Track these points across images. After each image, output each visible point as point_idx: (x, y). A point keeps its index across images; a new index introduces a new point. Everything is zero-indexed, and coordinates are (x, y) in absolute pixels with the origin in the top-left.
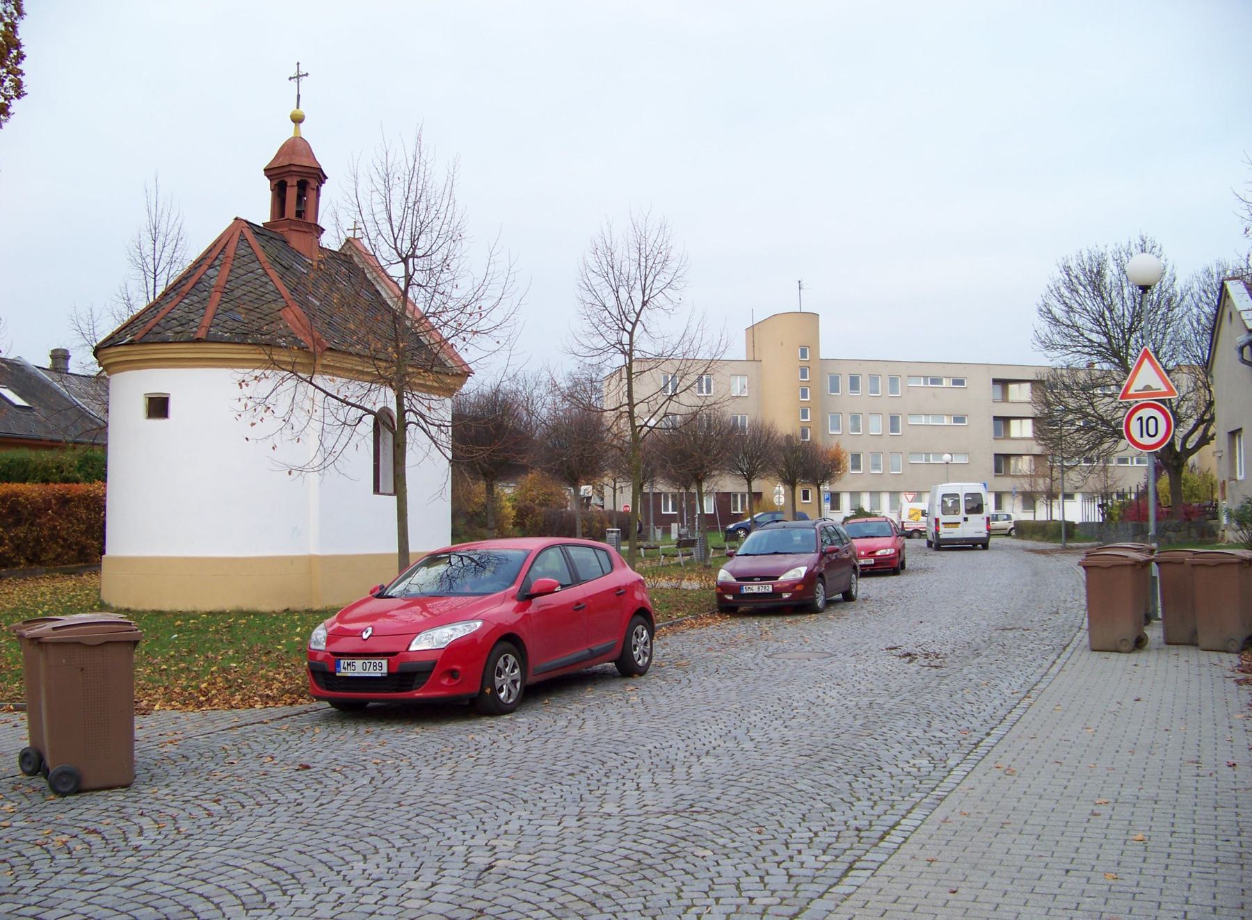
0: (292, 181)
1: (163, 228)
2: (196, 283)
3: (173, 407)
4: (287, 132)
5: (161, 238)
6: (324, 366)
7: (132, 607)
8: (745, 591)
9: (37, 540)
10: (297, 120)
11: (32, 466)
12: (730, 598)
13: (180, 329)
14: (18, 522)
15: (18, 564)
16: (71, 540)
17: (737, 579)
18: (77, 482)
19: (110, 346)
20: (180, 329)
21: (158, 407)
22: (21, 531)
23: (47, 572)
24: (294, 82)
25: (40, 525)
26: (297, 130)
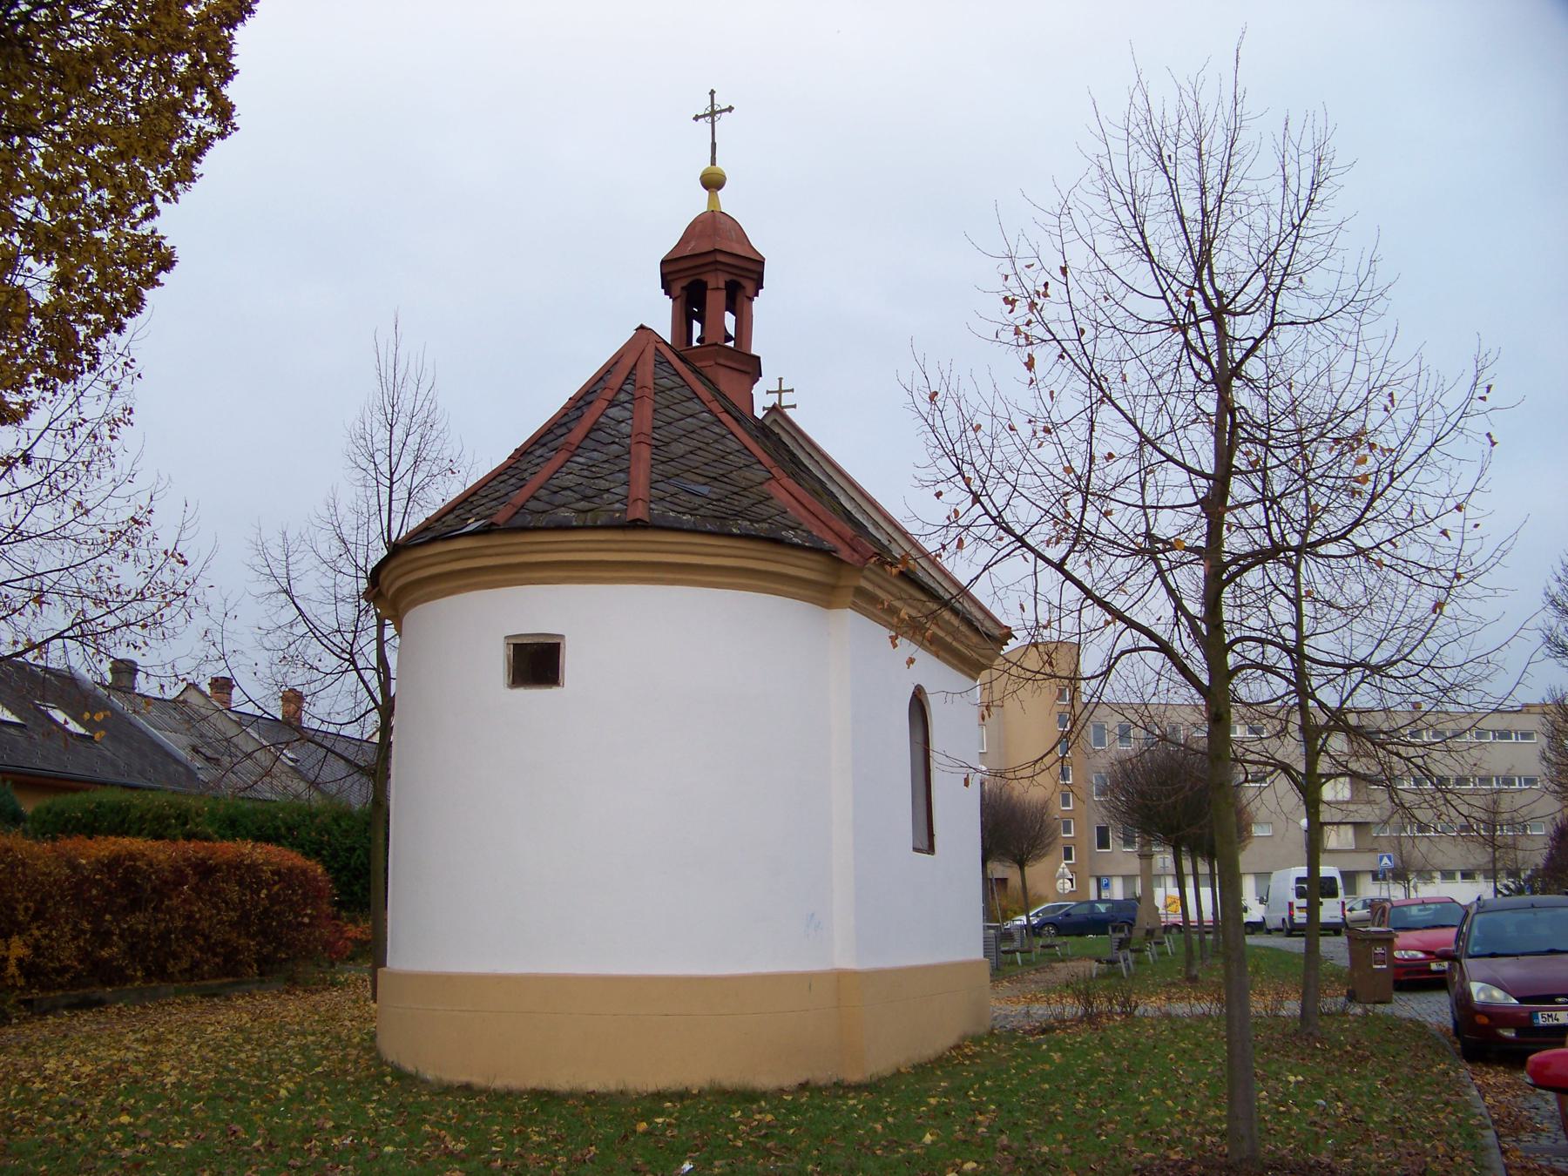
0: (717, 281)
1: (406, 405)
2: (592, 430)
3: (570, 662)
4: (697, 202)
5: (403, 420)
6: (860, 592)
7: (478, 1080)
8: (1541, 1020)
9: (164, 937)
10: (713, 182)
11: (135, 813)
12: (1509, 1033)
13: (583, 505)
14: (135, 905)
15: (132, 979)
16: (215, 937)
17: (1521, 1000)
18: (207, 838)
19: (434, 540)
20: (583, 505)
21: (536, 663)
22: (138, 921)
23: (177, 994)
24: (704, 125)
25: (169, 910)
26: (713, 200)
